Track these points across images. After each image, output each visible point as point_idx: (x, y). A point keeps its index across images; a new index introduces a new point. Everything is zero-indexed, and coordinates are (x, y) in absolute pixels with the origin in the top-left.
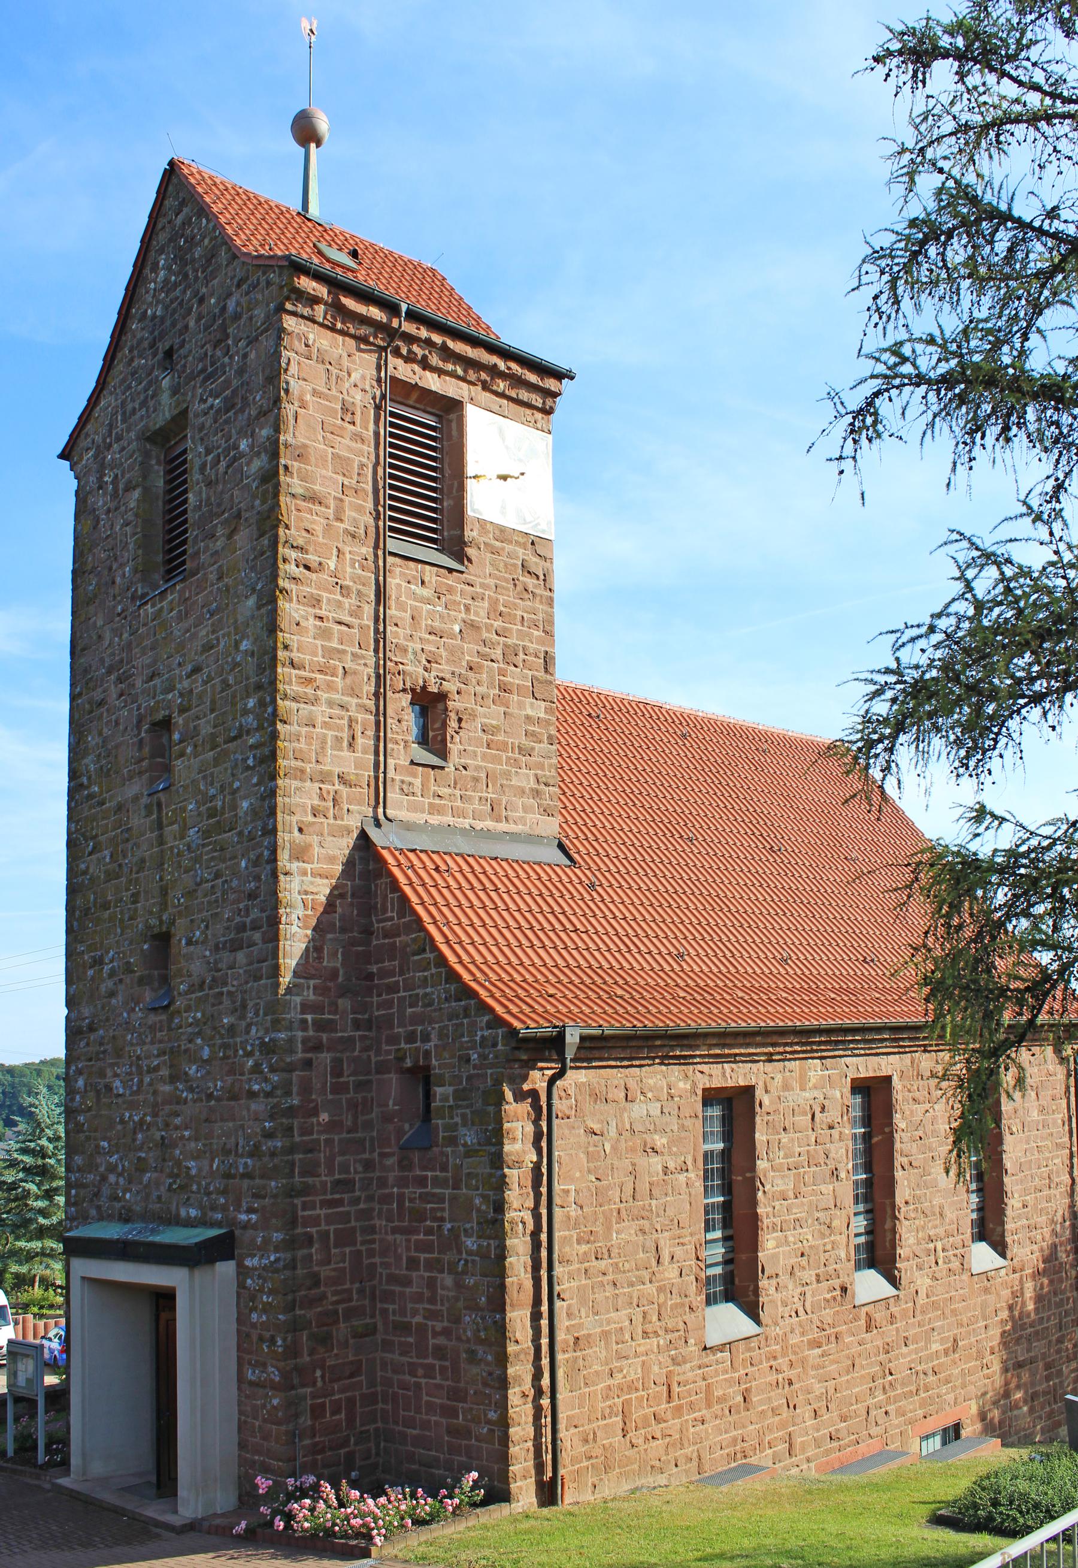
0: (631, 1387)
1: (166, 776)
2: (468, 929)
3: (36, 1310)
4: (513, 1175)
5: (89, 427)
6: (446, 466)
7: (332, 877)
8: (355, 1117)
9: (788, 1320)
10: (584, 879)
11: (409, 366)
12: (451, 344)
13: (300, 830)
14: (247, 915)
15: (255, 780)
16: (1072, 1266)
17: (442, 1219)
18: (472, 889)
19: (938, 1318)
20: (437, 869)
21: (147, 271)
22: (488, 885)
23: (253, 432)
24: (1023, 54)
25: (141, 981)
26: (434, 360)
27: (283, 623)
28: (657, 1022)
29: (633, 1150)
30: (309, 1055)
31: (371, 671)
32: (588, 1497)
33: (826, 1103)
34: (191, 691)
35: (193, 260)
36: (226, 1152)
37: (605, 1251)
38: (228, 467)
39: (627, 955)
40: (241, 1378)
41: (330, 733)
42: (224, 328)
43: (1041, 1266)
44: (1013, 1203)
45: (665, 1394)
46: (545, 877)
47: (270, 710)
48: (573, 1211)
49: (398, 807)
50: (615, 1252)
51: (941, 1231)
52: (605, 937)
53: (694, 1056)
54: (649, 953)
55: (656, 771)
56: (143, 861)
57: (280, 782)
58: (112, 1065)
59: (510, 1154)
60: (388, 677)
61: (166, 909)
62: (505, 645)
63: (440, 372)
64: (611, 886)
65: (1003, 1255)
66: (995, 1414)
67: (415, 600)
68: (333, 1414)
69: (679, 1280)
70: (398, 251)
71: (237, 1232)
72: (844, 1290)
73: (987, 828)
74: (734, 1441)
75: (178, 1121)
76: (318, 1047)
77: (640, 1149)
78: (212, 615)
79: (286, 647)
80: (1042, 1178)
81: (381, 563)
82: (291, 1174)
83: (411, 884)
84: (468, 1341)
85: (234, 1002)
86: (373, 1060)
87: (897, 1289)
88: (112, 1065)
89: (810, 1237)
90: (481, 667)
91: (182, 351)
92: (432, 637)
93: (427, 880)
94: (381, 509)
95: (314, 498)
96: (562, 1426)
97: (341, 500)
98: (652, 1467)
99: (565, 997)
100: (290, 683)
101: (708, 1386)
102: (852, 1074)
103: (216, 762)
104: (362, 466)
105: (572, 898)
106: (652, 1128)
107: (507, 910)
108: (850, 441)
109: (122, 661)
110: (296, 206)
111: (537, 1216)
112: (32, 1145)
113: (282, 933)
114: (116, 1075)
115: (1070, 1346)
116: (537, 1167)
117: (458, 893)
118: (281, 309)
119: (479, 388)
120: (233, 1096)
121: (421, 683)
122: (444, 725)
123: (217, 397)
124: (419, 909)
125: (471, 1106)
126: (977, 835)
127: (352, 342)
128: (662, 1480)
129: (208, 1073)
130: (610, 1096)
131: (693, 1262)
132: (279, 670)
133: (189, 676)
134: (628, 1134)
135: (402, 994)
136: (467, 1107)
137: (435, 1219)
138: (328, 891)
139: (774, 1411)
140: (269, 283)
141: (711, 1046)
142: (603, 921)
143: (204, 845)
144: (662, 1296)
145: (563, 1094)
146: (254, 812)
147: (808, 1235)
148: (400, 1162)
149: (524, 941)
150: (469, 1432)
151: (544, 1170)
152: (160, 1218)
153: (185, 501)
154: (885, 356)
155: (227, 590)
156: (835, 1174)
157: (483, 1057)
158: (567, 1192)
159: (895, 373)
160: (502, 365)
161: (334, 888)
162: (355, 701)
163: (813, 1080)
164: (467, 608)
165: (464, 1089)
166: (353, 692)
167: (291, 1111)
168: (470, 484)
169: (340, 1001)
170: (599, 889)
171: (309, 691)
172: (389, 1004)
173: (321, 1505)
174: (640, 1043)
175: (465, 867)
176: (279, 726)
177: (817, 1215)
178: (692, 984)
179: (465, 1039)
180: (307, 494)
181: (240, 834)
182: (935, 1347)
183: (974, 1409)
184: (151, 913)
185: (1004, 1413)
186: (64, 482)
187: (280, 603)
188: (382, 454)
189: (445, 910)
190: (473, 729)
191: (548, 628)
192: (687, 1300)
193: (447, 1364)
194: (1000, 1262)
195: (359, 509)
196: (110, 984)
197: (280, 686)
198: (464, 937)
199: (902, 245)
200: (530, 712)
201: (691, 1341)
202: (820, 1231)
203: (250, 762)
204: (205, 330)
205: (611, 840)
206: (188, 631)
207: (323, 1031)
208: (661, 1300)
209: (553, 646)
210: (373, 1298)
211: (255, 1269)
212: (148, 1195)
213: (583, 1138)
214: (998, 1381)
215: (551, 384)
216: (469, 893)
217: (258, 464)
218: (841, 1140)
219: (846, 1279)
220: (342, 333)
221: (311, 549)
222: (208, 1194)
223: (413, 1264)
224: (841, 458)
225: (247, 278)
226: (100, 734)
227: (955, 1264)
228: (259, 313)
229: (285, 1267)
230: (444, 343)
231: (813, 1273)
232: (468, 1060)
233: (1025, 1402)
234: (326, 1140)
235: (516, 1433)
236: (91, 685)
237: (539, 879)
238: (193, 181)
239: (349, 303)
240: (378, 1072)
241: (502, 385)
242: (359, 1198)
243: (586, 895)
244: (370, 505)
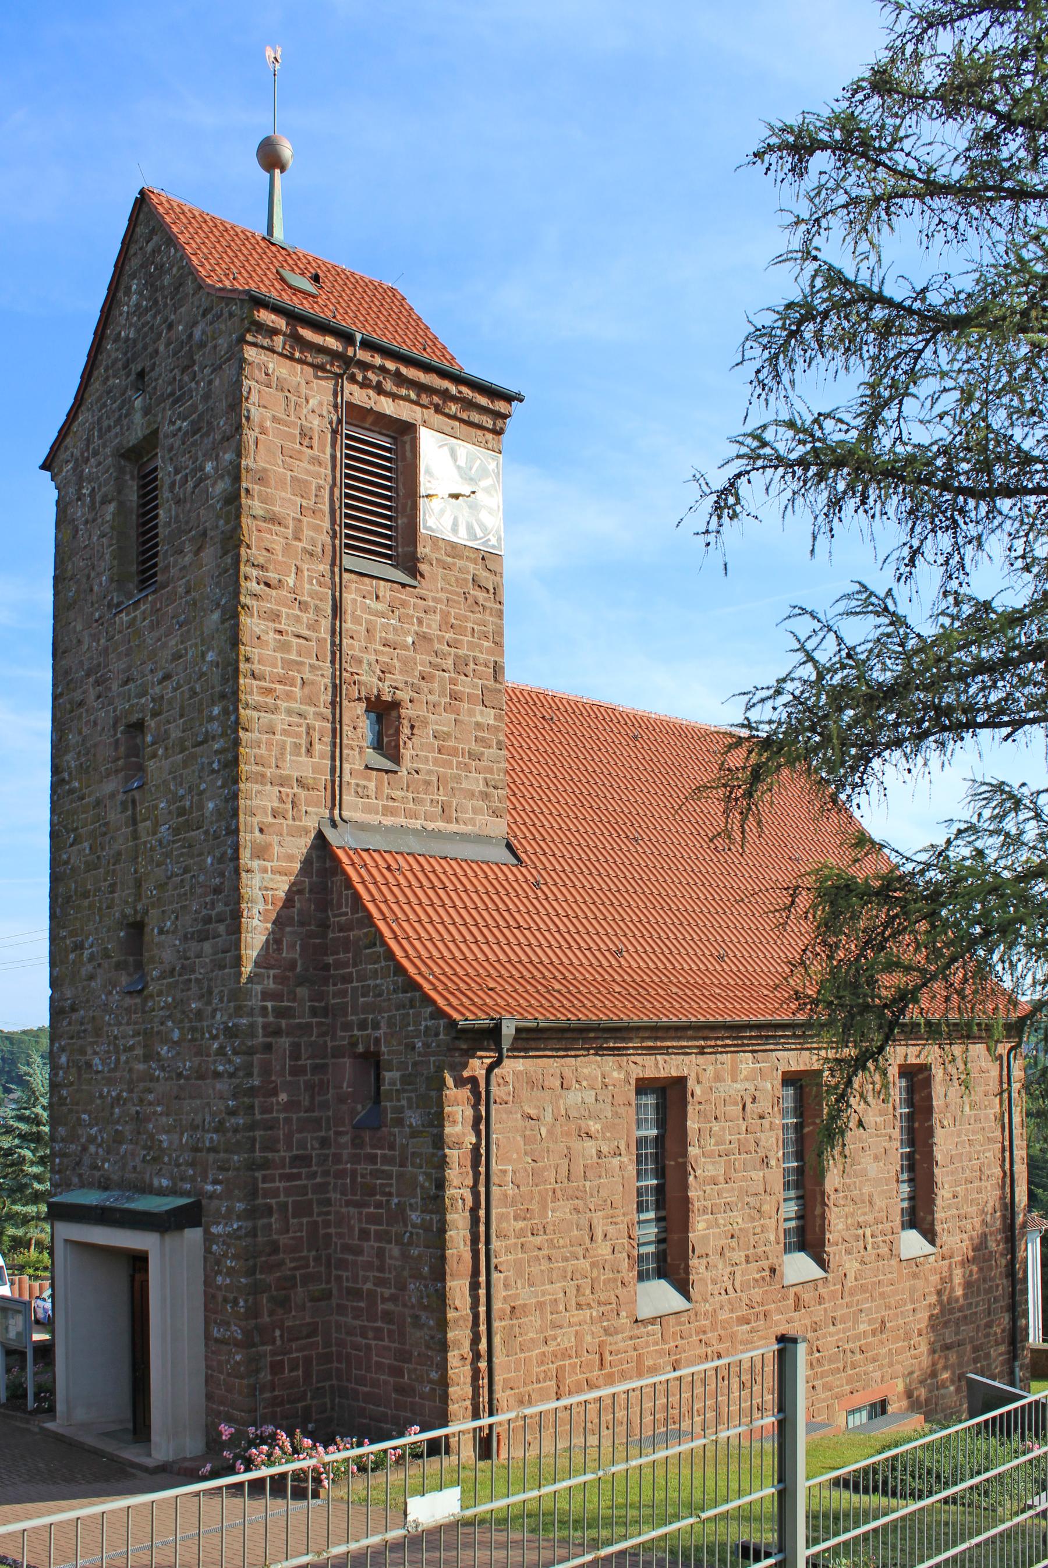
0: (565, 1354)
1: (140, 774)
2: (416, 925)
3: (31, 1271)
4: (453, 1155)
5: (68, 440)
6: (401, 486)
8: (312, 1097)
9: (717, 1298)
10: (529, 877)
11: (364, 392)
12: (404, 370)
13: (261, 830)
14: (213, 909)
15: (219, 783)
16: (1002, 1255)
17: (390, 1194)
18: (422, 886)
20: (389, 868)
21: (120, 294)
22: (437, 883)
23: (217, 455)
24: (896, 147)
25: (118, 966)
26: (389, 385)
27: (245, 637)
28: (591, 1016)
29: (568, 1134)
30: (269, 1040)
31: (328, 681)
33: (757, 1094)
34: (162, 697)
35: (163, 287)
36: (195, 1128)
37: (540, 1227)
38: (195, 487)
39: (567, 951)
40: (208, 1336)
41: (290, 740)
42: (190, 355)
43: (971, 1254)
44: (943, 1194)
45: (597, 1362)
46: (492, 876)
47: (233, 718)
48: (510, 1189)
49: (353, 809)
50: (550, 1228)
51: (870, 1218)
52: (546, 934)
53: (628, 1048)
54: (589, 949)
55: (606, 772)
56: (119, 854)
57: (242, 786)
58: (92, 1044)
59: (451, 1135)
60: (344, 687)
61: (140, 899)
62: (456, 656)
63: (395, 397)
64: (555, 884)
65: (932, 1242)
66: (922, 1393)
67: (370, 613)
68: (291, 1370)
69: (611, 1257)
70: (359, 272)
71: (204, 1202)
72: (773, 1270)
73: (866, 855)
75: (151, 1097)
76: (277, 1032)
77: (575, 1133)
78: (181, 626)
79: (248, 660)
80: (973, 1171)
81: (337, 580)
82: (252, 1150)
83: (363, 882)
84: (413, 1307)
85: (201, 989)
86: (329, 1044)
87: (826, 1271)
88: (92, 1044)
89: (740, 1221)
90: (433, 676)
91: (152, 374)
92: (387, 649)
93: (379, 878)
94: (337, 528)
95: (274, 519)
96: (498, 1387)
97: (300, 521)
99: (504, 990)
100: (251, 693)
101: (639, 1356)
102: (783, 1067)
103: (185, 764)
104: (319, 488)
105: (517, 896)
106: (586, 1114)
107: (454, 907)
108: (715, 518)
109: (99, 665)
110: (261, 231)
111: (476, 1194)
112: (27, 1112)
113: (244, 926)
114: (96, 1053)
115: (998, 1331)
116: (476, 1148)
117: (407, 891)
118: (242, 340)
119: (432, 411)
121: (375, 692)
122: (398, 732)
123: (184, 420)
124: (371, 906)
125: (415, 1090)
126: (857, 861)
127: (310, 370)
129: (178, 1054)
130: (546, 1084)
131: (625, 1241)
132: (241, 681)
133: (160, 682)
134: (563, 1119)
135: (355, 984)
136: (412, 1091)
137: (384, 1194)
138: (287, 888)
140: (231, 315)
141: (643, 1039)
142: (545, 918)
143: (174, 842)
144: (595, 1271)
145: (501, 1081)
146: (218, 812)
147: (738, 1219)
148: (353, 1140)
149: (469, 937)
150: (413, 1390)
151: (483, 1151)
152: (135, 1187)
153: (156, 516)
154: (749, 441)
155: (195, 604)
156: (765, 1161)
157: (426, 1045)
158: (505, 1172)
159: (757, 452)
160: (453, 389)
161: (293, 885)
162: (312, 709)
163: (745, 1073)
164: (420, 621)
165: (410, 1075)
166: (310, 701)
167: (252, 1091)
168: (422, 502)
169: (298, 990)
170: (544, 887)
171: (270, 700)
172: (343, 993)
173: (277, 1450)
174: (575, 1035)
175: (415, 866)
176: (241, 733)
178: (628, 979)
179: (411, 1028)
180: (267, 516)
181: (206, 832)
182: (863, 1327)
183: (900, 1387)
184: (126, 902)
185: (931, 1391)
186: (46, 492)
187: (242, 618)
188: (338, 475)
189: (394, 907)
190: (425, 736)
191: (497, 639)
193: (394, 1327)
194: (928, 1248)
195: (317, 529)
196: (90, 967)
197: (242, 696)
198: (411, 933)
199: (780, 323)
200: (479, 719)
201: (623, 1314)
203: (215, 766)
204: (174, 355)
205: (558, 840)
206: (159, 640)
207: (283, 1017)
208: (595, 1274)
209: (502, 655)
210: (329, 1265)
211: (220, 1236)
212: (124, 1165)
213: (520, 1123)
214: (926, 1361)
215: (501, 406)
216: (419, 891)
217: (221, 487)
218: (771, 1129)
219: (775, 1261)
220: (300, 361)
221: (271, 567)
222: (178, 1165)
223: (364, 1234)
224: (707, 532)
225: (212, 308)
226: (80, 733)
227: (884, 1250)
228: (223, 342)
229: (246, 1235)
230: (398, 369)
231: (743, 1254)
232: (414, 1048)
233: (952, 1382)
234: (285, 1119)
236: (72, 686)
237: (486, 877)
238: (161, 210)
239: (307, 334)
240: (334, 1056)
241: (454, 408)
242: (316, 1173)
243: (530, 893)
244: (326, 525)
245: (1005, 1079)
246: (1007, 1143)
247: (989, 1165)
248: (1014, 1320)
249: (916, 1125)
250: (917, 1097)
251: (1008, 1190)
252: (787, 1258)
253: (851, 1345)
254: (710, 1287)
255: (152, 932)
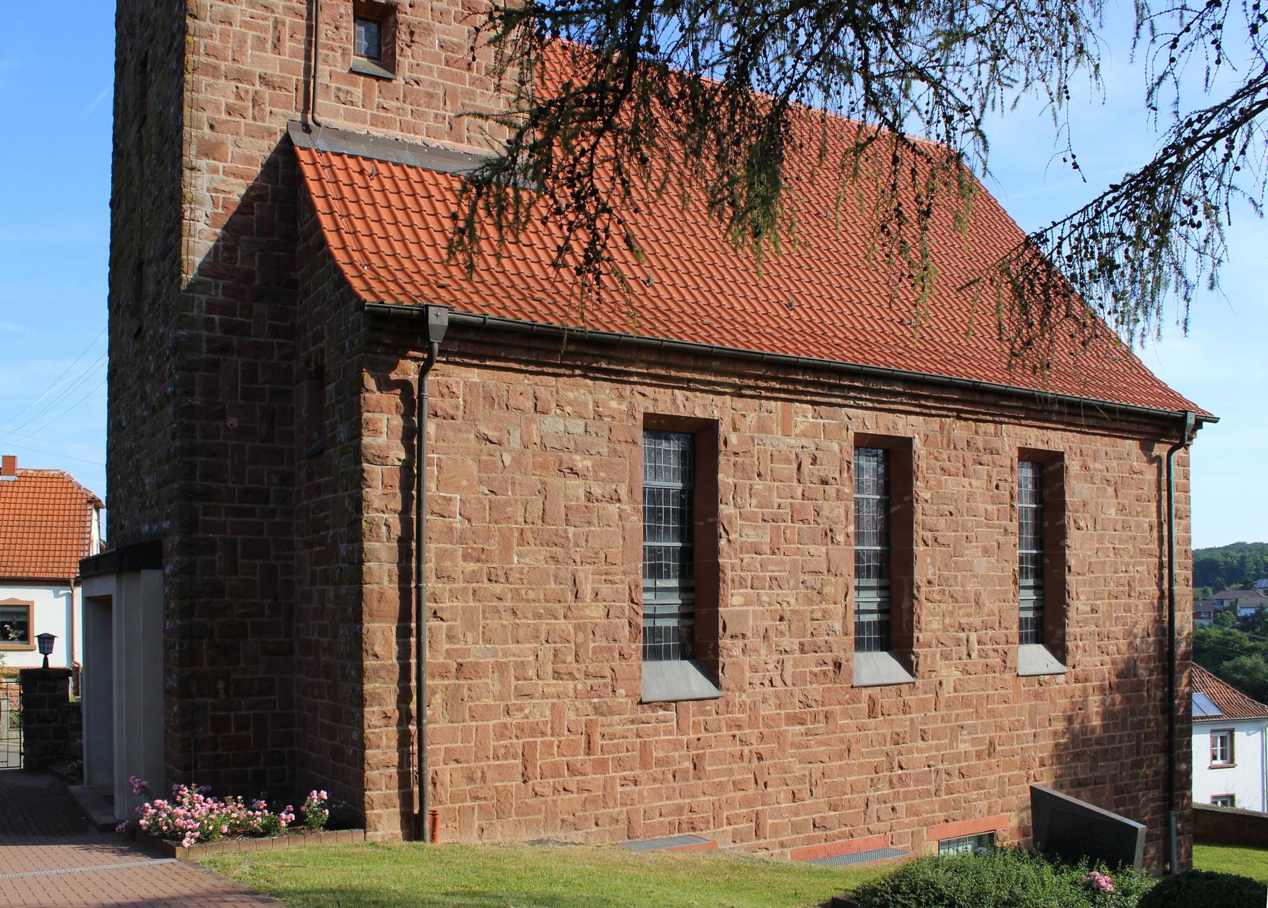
0: (536, 730)
4: (374, 472)
7: (249, 178)
9: (758, 689)
13: (212, 127)
19: (970, 716)
29: (544, 467)
30: (216, 356)
32: (473, 839)
33: (819, 454)
41: (251, 33)
43: (1114, 680)
48: (457, 522)
49: (329, 112)
50: (514, 576)
51: (976, 621)
53: (631, 374)
65: (1063, 660)
74: (679, 810)
76: (226, 349)
80: (1119, 584)
87: (913, 675)
89: (792, 601)
98: (563, 821)
101: (644, 744)
106: (572, 446)
113: (186, 228)
128: (577, 836)
130: (512, 403)
131: (626, 605)
138: (243, 191)
139: (737, 786)
141: (650, 364)
145: (445, 391)
156: (829, 534)
163: (801, 427)
169: (255, 305)
176: (189, 21)
177: (802, 577)
182: (963, 747)
192: (617, 645)
194: (1056, 666)
202: (806, 596)
213: (474, 443)
218: (838, 498)
219: (842, 655)
227: (995, 660)
231: (796, 641)
235: (374, 756)
245: (1164, 486)
246: (1165, 559)
247: (1141, 581)
248: (1171, 762)
249: (1046, 524)
250: (1046, 492)
251: (1166, 613)
252: (862, 656)
253: (946, 766)
254: (748, 675)
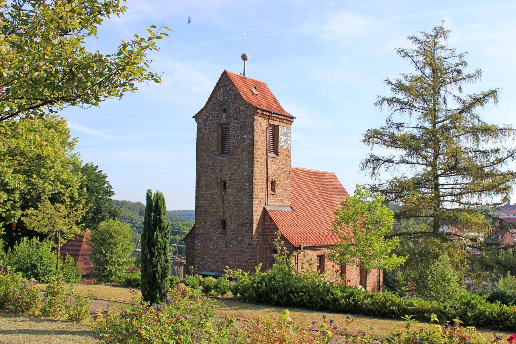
26: (275, 119)
36: (239, 261)
95: (258, 149)
103: (238, 192)
118: (254, 115)
120: (241, 251)
146: (248, 204)
239: (264, 113)
255: (228, 222)
